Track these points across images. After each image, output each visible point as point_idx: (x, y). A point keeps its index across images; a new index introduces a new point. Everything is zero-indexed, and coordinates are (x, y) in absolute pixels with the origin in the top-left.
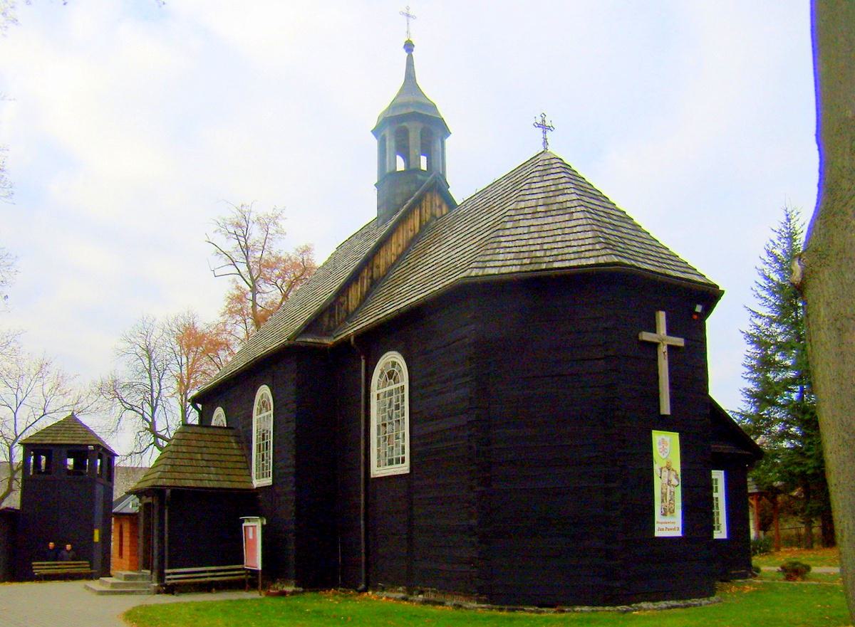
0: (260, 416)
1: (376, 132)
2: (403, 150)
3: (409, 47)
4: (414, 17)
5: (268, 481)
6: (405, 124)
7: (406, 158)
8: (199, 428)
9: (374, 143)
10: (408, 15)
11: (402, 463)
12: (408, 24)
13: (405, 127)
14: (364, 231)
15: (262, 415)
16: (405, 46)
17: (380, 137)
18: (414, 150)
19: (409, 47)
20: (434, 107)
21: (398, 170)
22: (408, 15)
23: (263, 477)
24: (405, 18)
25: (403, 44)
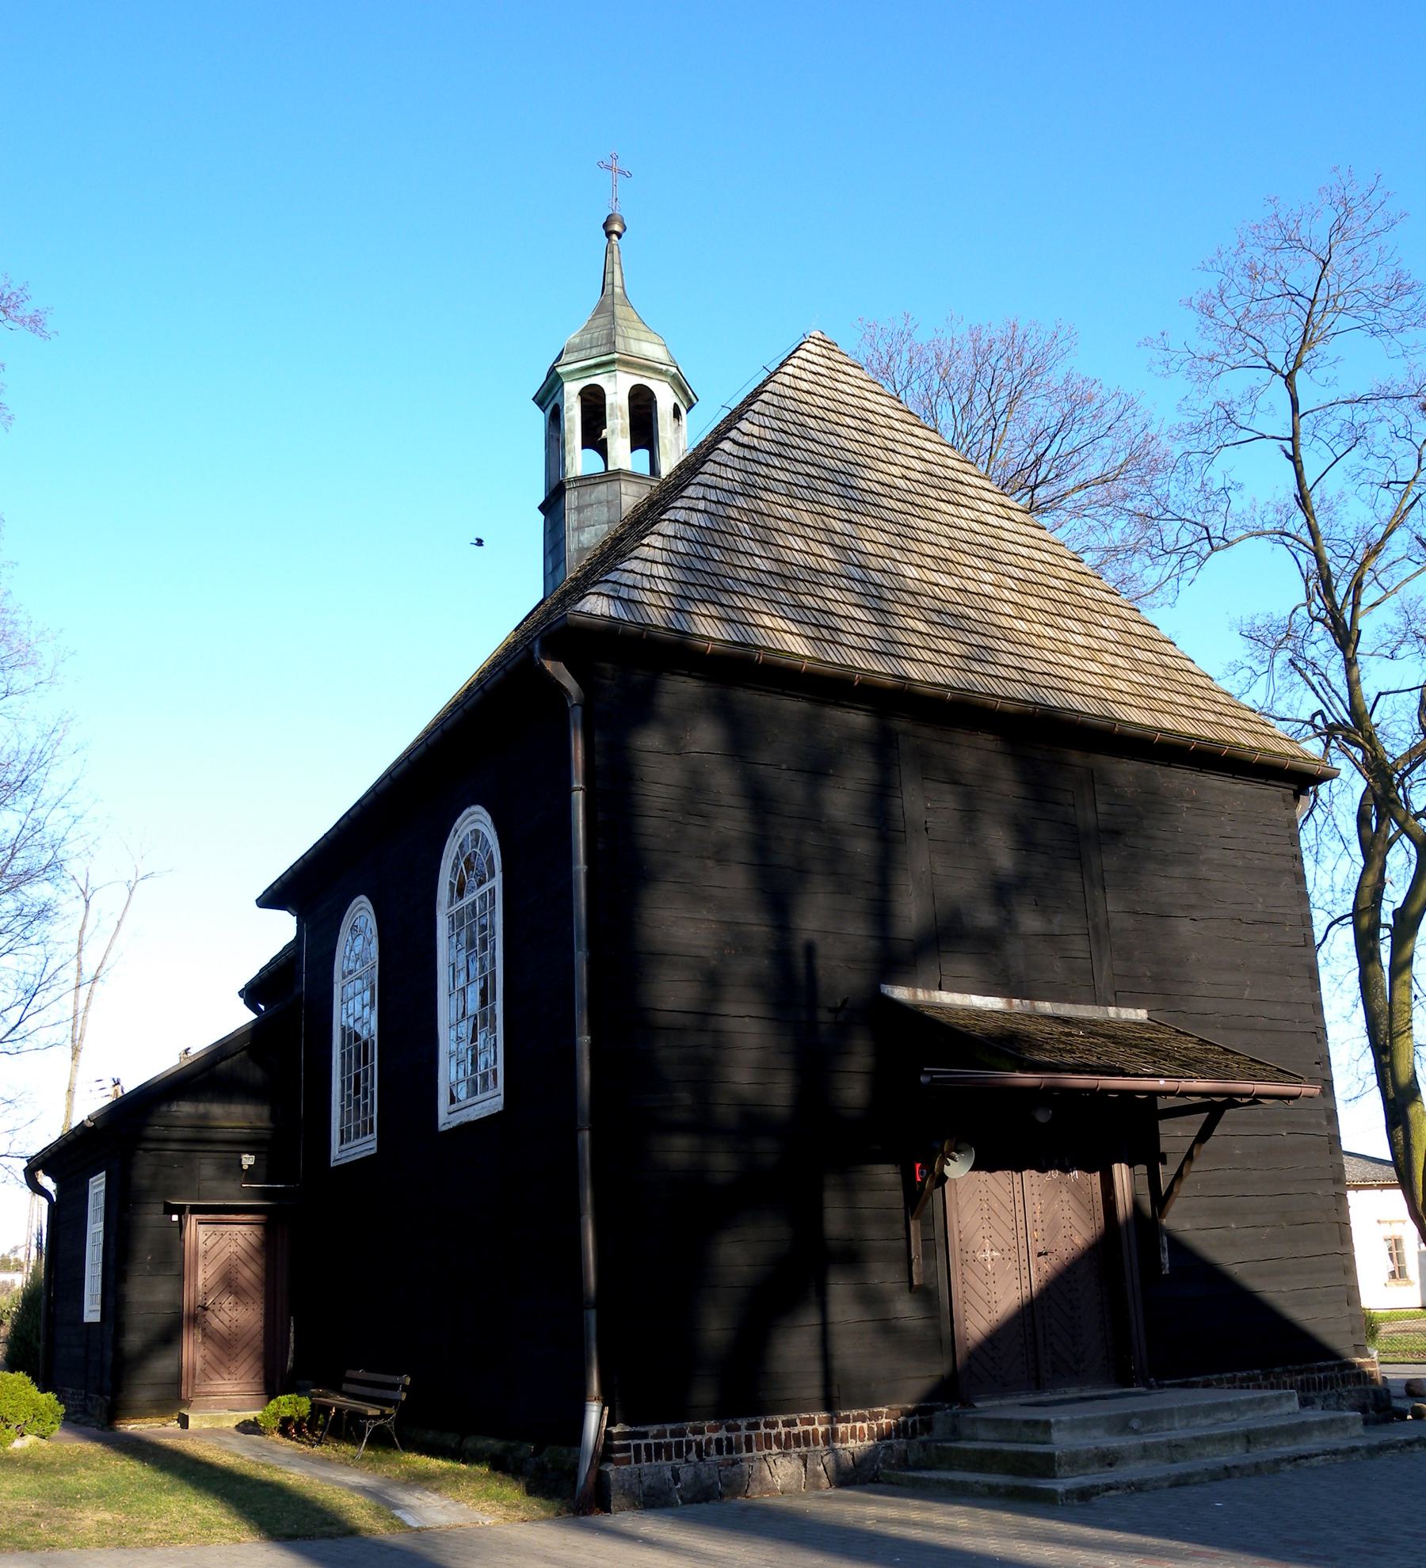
5: (367, 1145)
14: (550, 569)
15: (468, 899)
23: (357, 1136)
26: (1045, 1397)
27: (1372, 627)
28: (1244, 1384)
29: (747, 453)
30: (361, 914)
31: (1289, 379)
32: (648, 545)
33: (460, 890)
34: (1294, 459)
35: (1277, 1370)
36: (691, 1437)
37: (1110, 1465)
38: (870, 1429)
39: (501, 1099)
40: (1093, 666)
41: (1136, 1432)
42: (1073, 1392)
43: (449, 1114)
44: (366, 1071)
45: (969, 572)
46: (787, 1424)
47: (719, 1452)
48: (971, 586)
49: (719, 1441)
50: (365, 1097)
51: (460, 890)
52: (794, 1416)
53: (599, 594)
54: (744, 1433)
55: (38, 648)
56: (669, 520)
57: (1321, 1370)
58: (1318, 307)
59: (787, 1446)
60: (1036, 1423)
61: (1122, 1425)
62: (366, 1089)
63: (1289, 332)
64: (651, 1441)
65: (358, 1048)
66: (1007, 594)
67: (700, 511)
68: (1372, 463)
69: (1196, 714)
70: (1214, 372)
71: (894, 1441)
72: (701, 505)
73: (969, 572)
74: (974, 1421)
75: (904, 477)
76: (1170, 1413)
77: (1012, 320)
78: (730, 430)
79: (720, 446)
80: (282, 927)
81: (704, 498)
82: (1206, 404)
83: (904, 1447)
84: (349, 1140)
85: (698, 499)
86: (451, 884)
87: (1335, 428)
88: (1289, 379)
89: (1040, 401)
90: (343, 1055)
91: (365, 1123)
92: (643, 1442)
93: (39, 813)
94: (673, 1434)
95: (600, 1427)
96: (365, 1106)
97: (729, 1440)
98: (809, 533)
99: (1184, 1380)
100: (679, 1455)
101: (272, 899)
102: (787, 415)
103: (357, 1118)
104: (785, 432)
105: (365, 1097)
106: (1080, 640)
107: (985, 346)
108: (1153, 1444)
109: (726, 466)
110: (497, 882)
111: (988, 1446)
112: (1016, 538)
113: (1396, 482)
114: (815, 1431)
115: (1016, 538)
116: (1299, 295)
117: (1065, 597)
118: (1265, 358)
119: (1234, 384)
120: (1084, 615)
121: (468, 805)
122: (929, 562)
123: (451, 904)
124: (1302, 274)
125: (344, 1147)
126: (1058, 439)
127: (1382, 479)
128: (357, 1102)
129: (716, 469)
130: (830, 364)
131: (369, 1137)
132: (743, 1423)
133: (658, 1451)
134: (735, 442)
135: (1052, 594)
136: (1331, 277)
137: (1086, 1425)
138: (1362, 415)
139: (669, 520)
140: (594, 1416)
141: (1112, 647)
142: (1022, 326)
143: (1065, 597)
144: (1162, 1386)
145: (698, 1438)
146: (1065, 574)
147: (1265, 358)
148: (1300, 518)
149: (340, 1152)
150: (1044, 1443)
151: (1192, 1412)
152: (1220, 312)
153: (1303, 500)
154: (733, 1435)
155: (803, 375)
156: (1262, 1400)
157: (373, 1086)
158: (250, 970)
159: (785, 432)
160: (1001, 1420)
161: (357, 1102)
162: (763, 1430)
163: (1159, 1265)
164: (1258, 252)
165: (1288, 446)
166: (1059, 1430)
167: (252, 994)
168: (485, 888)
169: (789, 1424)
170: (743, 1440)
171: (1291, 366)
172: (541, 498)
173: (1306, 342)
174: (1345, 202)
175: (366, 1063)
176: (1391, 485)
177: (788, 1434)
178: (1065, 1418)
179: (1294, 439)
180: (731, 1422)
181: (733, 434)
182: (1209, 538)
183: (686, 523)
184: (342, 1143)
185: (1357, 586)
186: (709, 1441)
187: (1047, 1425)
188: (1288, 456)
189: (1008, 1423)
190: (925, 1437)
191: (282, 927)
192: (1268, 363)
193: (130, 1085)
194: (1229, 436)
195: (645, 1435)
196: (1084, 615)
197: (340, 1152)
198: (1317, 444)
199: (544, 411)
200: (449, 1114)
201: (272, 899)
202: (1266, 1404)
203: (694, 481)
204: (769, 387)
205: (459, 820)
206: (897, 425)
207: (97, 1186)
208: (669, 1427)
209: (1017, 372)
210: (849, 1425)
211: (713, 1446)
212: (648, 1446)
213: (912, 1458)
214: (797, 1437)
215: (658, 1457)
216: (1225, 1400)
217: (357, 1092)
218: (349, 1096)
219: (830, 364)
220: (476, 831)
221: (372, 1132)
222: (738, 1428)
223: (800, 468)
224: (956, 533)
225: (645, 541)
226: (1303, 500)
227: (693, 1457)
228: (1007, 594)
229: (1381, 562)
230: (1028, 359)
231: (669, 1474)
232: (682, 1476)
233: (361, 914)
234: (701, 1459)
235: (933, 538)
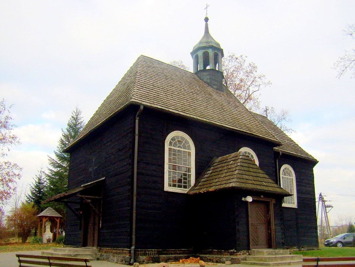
3: (207, 20)
16: (205, 19)
19: (207, 20)
20: (218, 45)
208: (107, 248)
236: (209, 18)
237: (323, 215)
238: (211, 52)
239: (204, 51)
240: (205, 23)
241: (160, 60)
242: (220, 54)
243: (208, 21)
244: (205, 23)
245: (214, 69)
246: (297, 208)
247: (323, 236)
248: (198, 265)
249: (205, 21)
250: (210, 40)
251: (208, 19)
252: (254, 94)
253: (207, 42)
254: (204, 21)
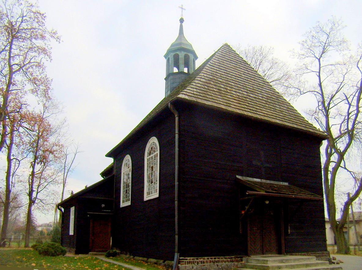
0: (149, 157)
1: (166, 56)
2: (177, 65)
3: (182, 21)
4: (185, 9)
5: (129, 203)
6: (177, 53)
7: (178, 68)
8: (190, 67)
9: (165, 61)
10: (182, 8)
11: (156, 192)
12: (182, 12)
13: (177, 54)
14: (166, 91)
15: (151, 156)
16: (180, 20)
17: (167, 59)
18: (182, 66)
19: (182, 21)
20: (191, 46)
21: (174, 72)
22: (182, 8)
23: (126, 202)
24: (181, 9)
25: (180, 19)
26: (264, 256)
27: (332, 112)
28: (304, 255)
29: (212, 67)
30: (128, 159)
31: (319, 60)
32: (192, 85)
33: (150, 154)
34: (319, 76)
35: (310, 253)
36: (196, 260)
37: (280, 268)
38: (230, 260)
39: (158, 195)
40: (281, 114)
41: (284, 263)
42: (270, 255)
43: (147, 197)
44: (128, 189)
45: (257, 94)
46: (214, 258)
47: (201, 263)
48: (257, 97)
49: (201, 261)
50: (128, 194)
51: (150, 154)
52: (219, 257)
53: (183, 94)
54: (206, 260)
55: (58, 105)
56: (197, 80)
57: (318, 253)
58: (326, 45)
59: (214, 263)
60: (265, 260)
61: (282, 261)
62: (128, 192)
63: (320, 49)
64: (188, 261)
65: (127, 185)
66: (264, 99)
67: (203, 78)
68: (334, 78)
69: (301, 125)
70: (304, 57)
71: (235, 263)
72: (203, 77)
73: (257, 94)
74: (252, 260)
75: (244, 74)
76: (291, 260)
77: (261, 46)
78: (208, 62)
79: (206, 65)
80: (111, 161)
81: (204, 76)
82: (301, 64)
83: (237, 264)
84: (124, 202)
85: (202, 76)
86: (148, 152)
87: (328, 70)
88: (319, 60)
89: (266, 63)
90: (123, 186)
91: (128, 199)
92: (186, 261)
93: (59, 138)
94: (192, 259)
95: (177, 258)
96: (128, 196)
97: (203, 261)
98: (225, 84)
99: (291, 254)
100: (193, 263)
101: (109, 155)
102: (220, 60)
103: (126, 198)
104: (220, 63)
105: (128, 194)
106: (278, 109)
107: (255, 51)
108: (288, 265)
109: (208, 70)
110: (158, 152)
111: (255, 264)
112: (266, 88)
113: (339, 82)
114: (220, 260)
115: (266, 88)
116: (322, 42)
117: (276, 100)
118: (314, 55)
119: (308, 60)
120: (280, 104)
121: (152, 137)
122: (249, 92)
123: (148, 156)
124: (324, 38)
125: (123, 203)
126: (269, 71)
127: (335, 82)
128: (126, 195)
129: (205, 70)
130: (229, 50)
131: (129, 202)
132: (206, 258)
133: (189, 263)
134: (211, 62)
135: (273, 99)
136: (329, 39)
137: (275, 261)
138: (333, 68)
139: (197, 80)
140: (289, 231)
141: (285, 111)
142: (263, 47)
143: (276, 100)
144: (287, 255)
145: (197, 260)
146: (276, 96)
147: (314, 55)
148: (319, 88)
149: (122, 205)
150: (266, 264)
151: (295, 260)
152: (306, 45)
153: (320, 85)
154: (204, 260)
155: (223, 52)
156: (309, 258)
157: (130, 192)
158: (102, 170)
159: (220, 63)
160: (257, 260)
161: (126, 195)
162: (210, 259)
163: (288, 232)
164: (314, 33)
165: (318, 74)
166: (269, 262)
167: (103, 174)
168: (156, 153)
169: (215, 258)
170: (206, 261)
171: (320, 56)
172: (165, 77)
173: (323, 53)
174: (333, 23)
175: (128, 187)
176: (337, 83)
177: (215, 260)
178: (271, 259)
179: (319, 73)
180: (204, 258)
181: (209, 63)
182: (300, 92)
183: (200, 81)
184: (123, 203)
185: (329, 104)
186: (199, 261)
187: (267, 261)
188: (318, 76)
189: (259, 260)
190: (241, 262)
191: (111, 161)
192: (315, 56)
193: (75, 192)
194: (306, 71)
195: (187, 259)
196: (280, 104)
197: (122, 205)
198: (324, 73)
199: (166, 59)
200: (147, 197)
201: (109, 155)
202: (309, 259)
203: (201, 72)
204: (216, 54)
205: (150, 140)
206: (242, 63)
207: (73, 209)
208: (192, 258)
209: (262, 57)
210: (227, 259)
211: (200, 262)
212: (187, 262)
213: (239, 266)
214: (216, 261)
215: (189, 264)
216: (302, 258)
217: (126, 193)
218: (124, 194)
219: (229, 50)
220: (153, 142)
221: (129, 200)
222: (205, 259)
223: (223, 71)
224: (254, 86)
225: (192, 84)
226: (320, 85)
227: (196, 264)
228: (264, 99)
229: (334, 99)
230: (264, 54)
231: (191, 267)
232: (194, 267)
233: (128, 159)
234: (198, 264)
235: (249, 87)
236: (184, 20)
237: (66, 175)
238: (182, 55)
239: (186, 53)
240: (346, 170)
241: (211, 55)
242: (192, 57)
243: (183, 22)
244: (180, 23)
245: (14, 71)
246: (121, 207)
247: (57, 181)
248: (153, 269)
249: (181, 22)
250: (183, 42)
251: (184, 21)
252: (316, 123)
253: (180, 44)
254: (179, 22)
